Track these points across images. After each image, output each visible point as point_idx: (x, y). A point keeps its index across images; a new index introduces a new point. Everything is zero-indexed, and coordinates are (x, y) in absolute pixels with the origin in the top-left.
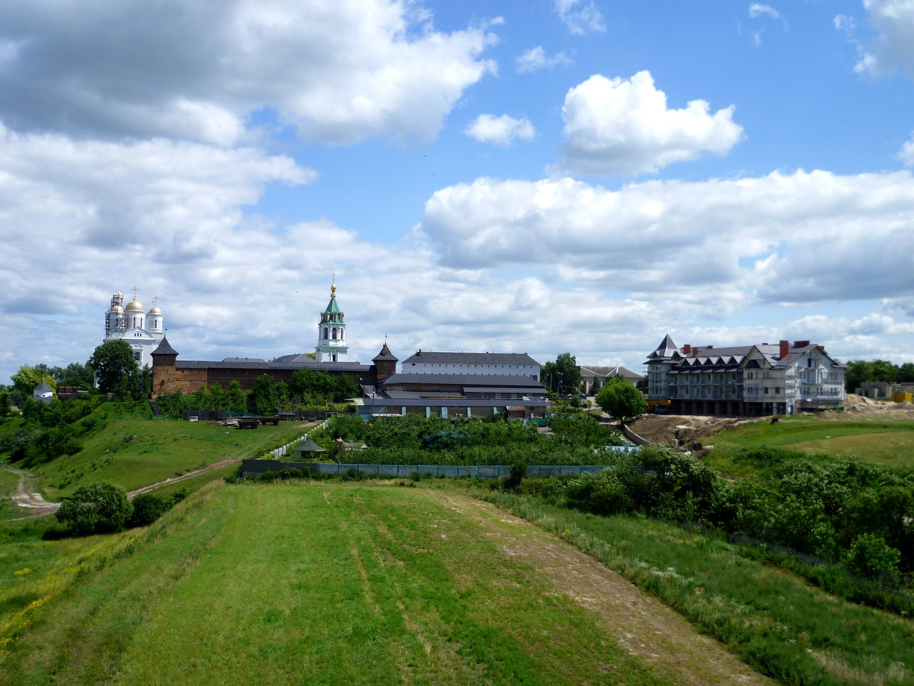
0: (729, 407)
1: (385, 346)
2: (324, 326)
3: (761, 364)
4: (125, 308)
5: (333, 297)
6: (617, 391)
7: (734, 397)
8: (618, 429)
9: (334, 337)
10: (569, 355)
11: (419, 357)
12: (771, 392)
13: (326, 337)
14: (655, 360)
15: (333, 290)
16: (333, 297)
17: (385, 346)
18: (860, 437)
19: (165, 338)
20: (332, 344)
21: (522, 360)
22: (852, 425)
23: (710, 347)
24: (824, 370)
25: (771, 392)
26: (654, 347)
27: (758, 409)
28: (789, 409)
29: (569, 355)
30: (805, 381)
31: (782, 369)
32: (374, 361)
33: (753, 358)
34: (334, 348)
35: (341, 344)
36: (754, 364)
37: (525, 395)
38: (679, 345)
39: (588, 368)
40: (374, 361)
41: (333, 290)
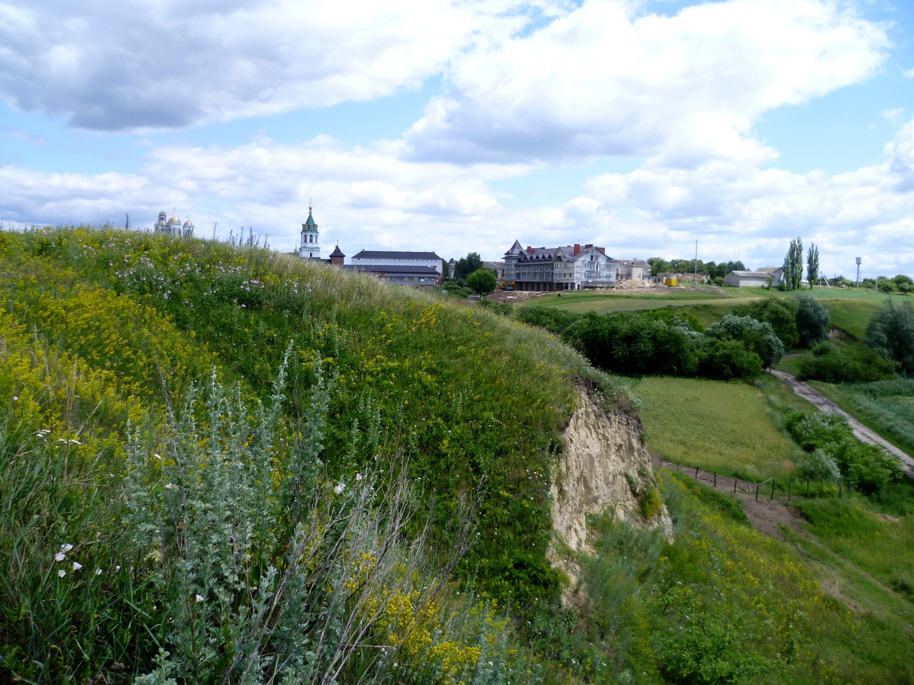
0: (548, 285)
1: (337, 247)
2: (304, 234)
3: (563, 259)
4: (894, 363)
5: (310, 213)
6: (478, 275)
7: (550, 280)
8: (743, 369)
9: (311, 241)
10: (476, 253)
11: (363, 255)
12: (568, 276)
13: (306, 241)
14: (508, 256)
15: (310, 209)
16: (310, 213)
17: (337, 247)
18: (605, 301)
19: (310, 218)
20: (309, 245)
21: (432, 256)
22: (607, 296)
23: (544, 248)
24: (602, 261)
25: (568, 276)
26: (508, 248)
27: (561, 286)
28: (576, 287)
29: (476, 253)
30: (589, 270)
31: (573, 262)
32: (330, 256)
33: (558, 255)
34: (310, 248)
35: (315, 245)
36: (559, 259)
37: (423, 278)
38: (525, 248)
39: (495, 263)
40: (330, 256)
41: (310, 209)
